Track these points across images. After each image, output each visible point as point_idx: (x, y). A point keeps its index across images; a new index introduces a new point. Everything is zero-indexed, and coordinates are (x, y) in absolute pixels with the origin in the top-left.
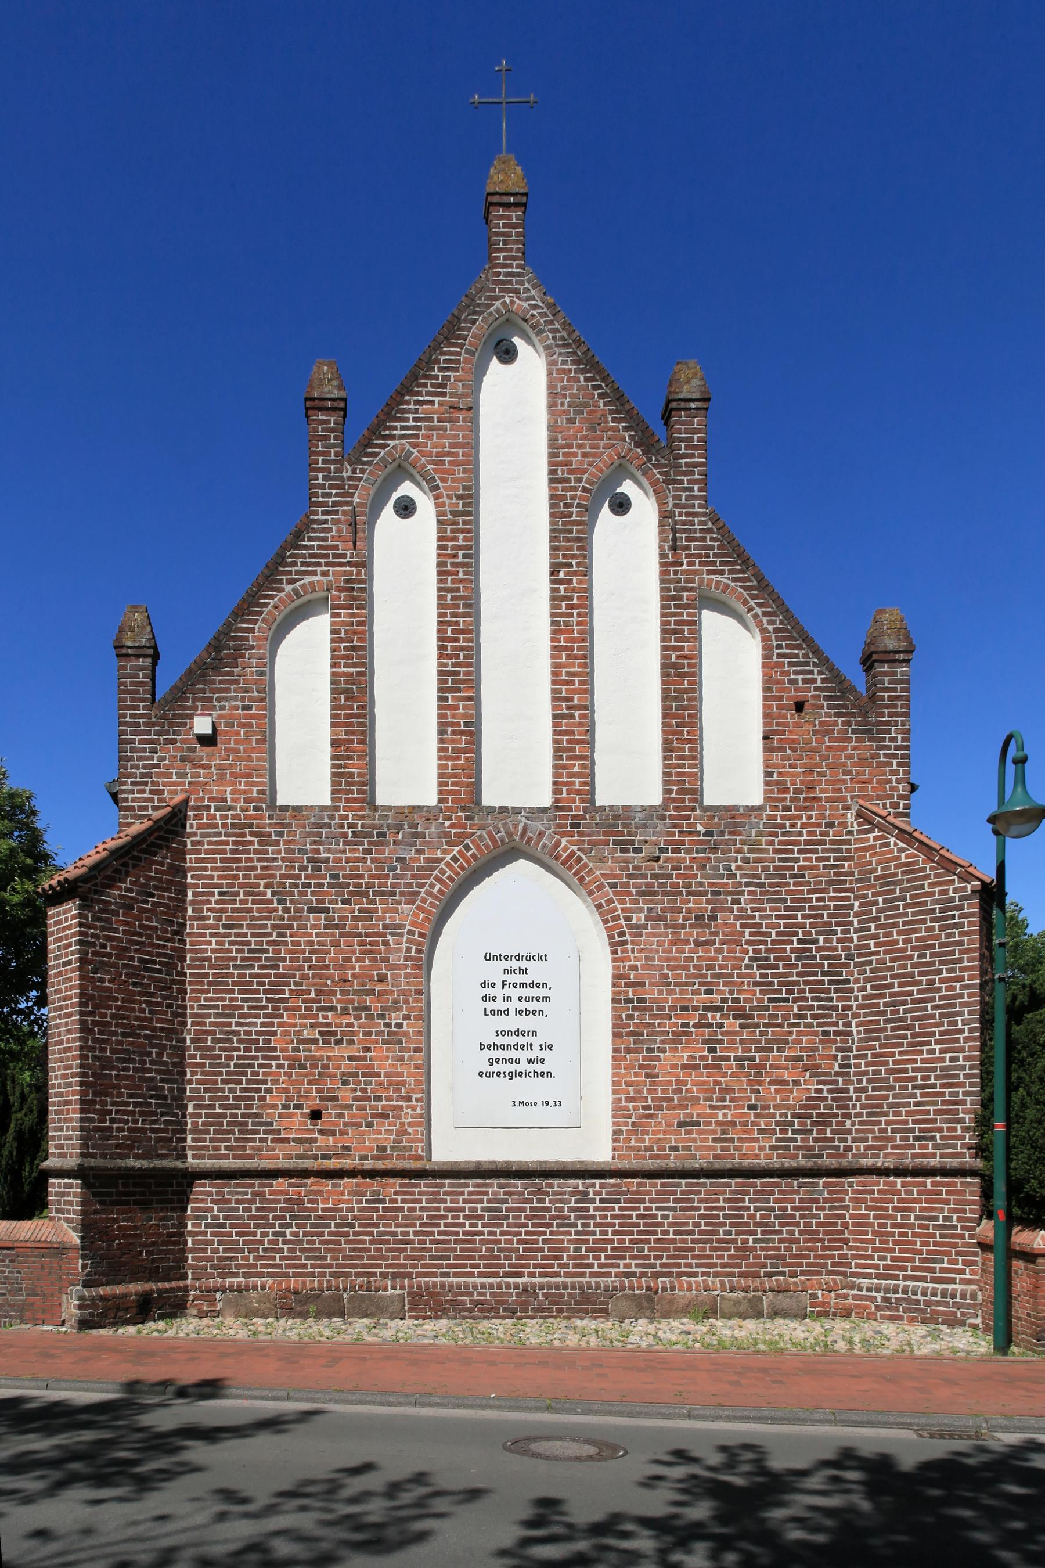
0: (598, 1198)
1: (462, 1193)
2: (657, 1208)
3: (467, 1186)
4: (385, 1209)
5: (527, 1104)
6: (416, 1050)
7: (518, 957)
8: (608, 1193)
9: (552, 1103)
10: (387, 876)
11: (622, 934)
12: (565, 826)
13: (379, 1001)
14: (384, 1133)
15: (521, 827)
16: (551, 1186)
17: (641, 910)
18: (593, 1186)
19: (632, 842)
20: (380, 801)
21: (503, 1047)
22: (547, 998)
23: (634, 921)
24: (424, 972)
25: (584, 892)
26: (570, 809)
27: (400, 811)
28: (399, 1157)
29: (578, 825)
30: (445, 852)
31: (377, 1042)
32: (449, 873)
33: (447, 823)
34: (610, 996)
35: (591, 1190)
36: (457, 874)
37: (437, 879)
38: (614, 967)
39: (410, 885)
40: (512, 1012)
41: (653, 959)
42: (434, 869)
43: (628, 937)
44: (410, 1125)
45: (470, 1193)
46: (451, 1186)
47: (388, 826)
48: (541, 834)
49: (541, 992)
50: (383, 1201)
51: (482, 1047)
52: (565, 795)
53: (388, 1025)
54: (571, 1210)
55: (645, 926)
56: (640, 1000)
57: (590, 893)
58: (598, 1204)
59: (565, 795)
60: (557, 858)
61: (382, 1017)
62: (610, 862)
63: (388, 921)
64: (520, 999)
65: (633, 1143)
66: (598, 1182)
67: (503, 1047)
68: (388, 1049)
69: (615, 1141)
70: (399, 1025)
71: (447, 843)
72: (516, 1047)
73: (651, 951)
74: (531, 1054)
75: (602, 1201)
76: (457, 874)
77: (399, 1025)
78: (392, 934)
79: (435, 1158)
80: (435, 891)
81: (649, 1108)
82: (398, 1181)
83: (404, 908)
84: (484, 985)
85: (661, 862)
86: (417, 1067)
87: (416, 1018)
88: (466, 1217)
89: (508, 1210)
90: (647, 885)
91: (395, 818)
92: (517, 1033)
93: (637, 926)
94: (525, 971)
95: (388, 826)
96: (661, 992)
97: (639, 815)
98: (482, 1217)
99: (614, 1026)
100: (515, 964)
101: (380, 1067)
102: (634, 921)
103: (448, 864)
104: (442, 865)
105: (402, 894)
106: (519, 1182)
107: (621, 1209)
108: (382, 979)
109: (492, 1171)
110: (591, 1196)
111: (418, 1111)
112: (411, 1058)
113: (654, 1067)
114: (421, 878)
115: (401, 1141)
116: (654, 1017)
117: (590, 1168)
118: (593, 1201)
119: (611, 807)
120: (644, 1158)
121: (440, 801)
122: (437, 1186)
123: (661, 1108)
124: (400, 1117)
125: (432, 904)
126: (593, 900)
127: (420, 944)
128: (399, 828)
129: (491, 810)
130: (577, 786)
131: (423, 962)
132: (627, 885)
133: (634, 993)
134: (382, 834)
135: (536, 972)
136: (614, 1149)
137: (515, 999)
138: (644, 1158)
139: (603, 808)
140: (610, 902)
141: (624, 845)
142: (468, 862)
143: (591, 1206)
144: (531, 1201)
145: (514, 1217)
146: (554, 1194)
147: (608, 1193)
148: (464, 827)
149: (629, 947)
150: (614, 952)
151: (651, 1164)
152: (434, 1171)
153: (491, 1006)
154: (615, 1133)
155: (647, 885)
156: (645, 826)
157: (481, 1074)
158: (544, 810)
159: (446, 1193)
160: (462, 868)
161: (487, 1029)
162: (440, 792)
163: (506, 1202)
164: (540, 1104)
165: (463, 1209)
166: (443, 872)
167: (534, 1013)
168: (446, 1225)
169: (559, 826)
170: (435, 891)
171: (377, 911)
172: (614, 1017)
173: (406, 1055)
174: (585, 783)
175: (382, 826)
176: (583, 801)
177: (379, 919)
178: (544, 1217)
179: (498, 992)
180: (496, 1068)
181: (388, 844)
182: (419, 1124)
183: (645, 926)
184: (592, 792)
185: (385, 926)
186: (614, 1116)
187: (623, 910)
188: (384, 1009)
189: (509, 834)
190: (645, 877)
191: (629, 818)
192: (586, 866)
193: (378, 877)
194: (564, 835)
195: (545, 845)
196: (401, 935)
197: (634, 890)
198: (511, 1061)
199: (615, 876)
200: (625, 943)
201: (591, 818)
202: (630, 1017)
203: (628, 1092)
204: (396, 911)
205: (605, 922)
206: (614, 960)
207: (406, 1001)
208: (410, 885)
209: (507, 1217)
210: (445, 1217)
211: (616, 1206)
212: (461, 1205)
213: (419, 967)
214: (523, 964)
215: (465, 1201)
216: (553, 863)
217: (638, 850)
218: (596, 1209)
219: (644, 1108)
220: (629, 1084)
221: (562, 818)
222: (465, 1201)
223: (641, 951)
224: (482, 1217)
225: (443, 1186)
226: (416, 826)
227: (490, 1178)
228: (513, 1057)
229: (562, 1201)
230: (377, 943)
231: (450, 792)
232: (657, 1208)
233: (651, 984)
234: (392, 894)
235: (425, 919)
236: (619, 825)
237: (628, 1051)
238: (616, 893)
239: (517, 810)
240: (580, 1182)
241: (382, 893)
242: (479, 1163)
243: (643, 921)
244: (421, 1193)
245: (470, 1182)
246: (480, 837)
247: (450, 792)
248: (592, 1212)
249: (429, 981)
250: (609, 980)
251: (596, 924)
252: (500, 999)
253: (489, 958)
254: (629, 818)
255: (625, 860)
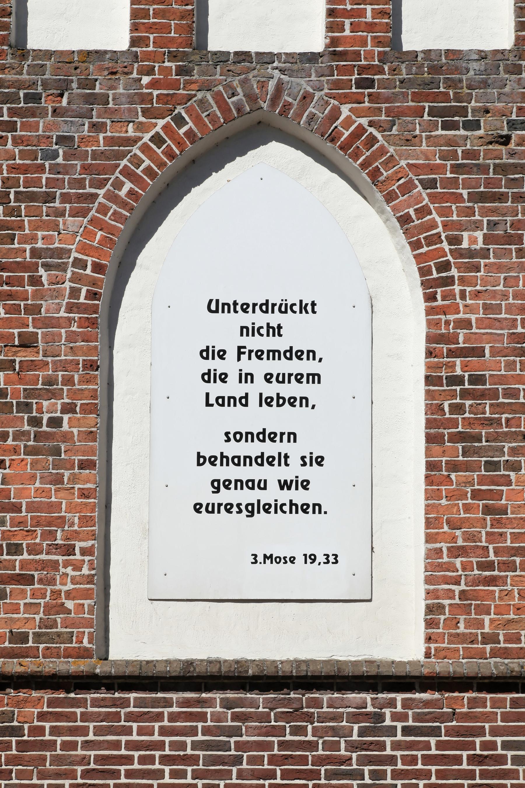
0: (399, 725)
1: (159, 717)
2: (506, 746)
3: (168, 703)
4: (22, 746)
5: (278, 560)
6: (82, 465)
7: (266, 307)
8: (417, 718)
9: (321, 558)
10: (41, 169)
11: (445, 266)
12: (348, 84)
13: (21, 381)
14: (23, 609)
15: (272, 85)
16: (318, 703)
17: (477, 226)
18: (392, 703)
19: (463, 111)
20: (34, 42)
21: (237, 460)
22: (315, 378)
23: (465, 245)
24: (101, 332)
25: (379, 196)
26: (357, 56)
27: (67, 60)
28: (49, 653)
29: (370, 84)
30: (141, 128)
31: (15, 451)
32: (147, 162)
33: (146, 80)
34: (421, 372)
35: (387, 712)
36: (161, 165)
37: (127, 173)
38: (429, 323)
39: (80, 184)
40: (254, 400)
41: (498, 309)
42: (121, 156)
43: (454, 272)
44: (69, 595)
45: (173, 717)
46: (139, 703)
47: (45, 85)
48: (306, 98)
49: (305, 367)
50: (17, 731)
51: (201, 460)
52: (347, 33)
53: (36, 422)
54: (353, 747)
55: (484, 254)
56: (475, 380)
57: (390, 198)
58: (399, 737)
59: (347, 33)
60: (333, 140)
61: (26, 407)
62: (427, 145)
63: (40, 245)
64: (268, 378)
65: (462, 628)
66: (399, 697)
67: (237, 460)
68: (34, 464)
69: (430, 624)
70: (55, 422)
71: (145, 113)
72: (261, 460)
73: (494, 295)
74: (286, 473)
75: (406, 731)
76: (161, 165)
77: (55, 422)
78: (47, 267)
79: (114, 654)
80: (123, 193)
81: (490, 566)
82: (47, 695)
83: (71, 222)
84: (206, 353)
85: (512, 145)
86: (84, 494)
87: (85, 409)
88: (166, 760)
89: (239, 746)
90: (488, 183)
91: (56, 71)
92: (263, 436)
93: (471, 253)
94: (276, 331)
95: (45, 85)
96: (511, 366)
97: (475, 66)
98: (193, 760)
99: (429, 424)
100: (260, 319)
101: (19, 493)
102: (465, 245)
103: (145, 149)
104: (136, 150)
105: (65, 198)
106: (260, 698)
107: (440, 745)
108: (27, 343)
109: (212, 677)
110: (388, 722)
111: (85, 571)
112: (74, 479)
113: (499, 495)
114: (98, 173)
115: (54, 624)
116: (498, 408)
117: (384, 671)
118: (391, 731)
119: (427, 52)
120: (482, 655)
121: (134, 42)
122: (115, 703)
123: (511, 566)
124: (52, 582)
125: (116, 216)
126: (395, 209)
127: (94, 283)
128: (62, 88)
129: (221, 57)
130: (369, 18)
131: (101, 313)
132: (454, 183)
133: (465, 367)
134: (35, 98)
135: (296, 331)
136: (429, 639)
137: (259, 378)
138: (482, 655)
139: (415, 54)
140: (423, 211)
141: (449, 117)
142: (180, 144)
143: (388, 740)
144: (281, 732)
145: (252, 760)
146: (323, 718)
147: (417, 718)
148: (175, 85)
149: (457, 288)
150: (430, 298)
151: (494, 666)
152: (109, 677)
153: (217, 389)
154: (429, 609)
155: (488, 183)
156: (485, 84)
157: (197, 508)
158: (311, 58)
159: (130, 717)
160: (171, 155)
161: (211, 430)
162: (135, 28)
163: (236, 732)
164: (300, 559)
165: (160, 746)
166: (138, 163)
167: (292, 401)
168: (129, 774)
169: (337, 85)
170: (123, 193)
171: (21, 228)
172: (430, 409)
173: (67, 474)
174: (383, 13)
175: (35, 83)
176: (378, 42)
177: (24, 240)
178: (303, 760)
179: (230, 365)
180: (226, 496)
181: (43, 114)
182: (86, 594)
183: (484, 254)
184: (396, 27)
185: (35, 253)
186: (428, 580)
187: (445, 225)
188: (29, 393)
189: (251, 98)
190: (485, 169)
191: (457, 70)
192: (382, 151)
193: (25, 170)
194: (345, 99)
195: (312, 117)
196: (63, 268)
197: (465, 193)
198: (251, 484)
199: (433, 169)
200: (450, 281)
201: (393, 71)
202: (457, 409)
203: (454, 539)
204: (55, 227)
205: (415, 245)
206: (429, 311)
207: (68, 381)
208: (80, 184)
209: (238, 760)
210: (129, 760)
211: (433, 741)
212: (156, 737)
213: (93, 323)
214: (275, 319)
215: (163, 732)
216: (327, 147)
217: (474, 125)
218: (396, 746)
219: (481, 566)
220: (453, 525)
221: (342, 71)
222: (163, 732)
223: (477, 295)
224: (193, 760)
225: (125, 703)
226: (92, 85)
227: (208, 690)
228: (254, 478)
229: (335, 732)
230: (20, 282)
231: (150, 28)
232: (506, 746)
233: (494, 352)
234: (49, 198)
235: (104, 241)
236: (443, 83)
237: (454, 467)
238: (433, 198)
239: (266, 58)
240: (368, 697)
241: (31, 197)
242: (190, 663)
243: (480, 244)
244: (85, 717)
245: (174, 696)
246: (202, 102)
247: (150, 28)
248: (388, 751)
249: (111, 347)
250: (420, 346)
251: (401, 250)
252: (232, 378)
253: (215, 307)
254: (457, 70)
255: (451, 142)
